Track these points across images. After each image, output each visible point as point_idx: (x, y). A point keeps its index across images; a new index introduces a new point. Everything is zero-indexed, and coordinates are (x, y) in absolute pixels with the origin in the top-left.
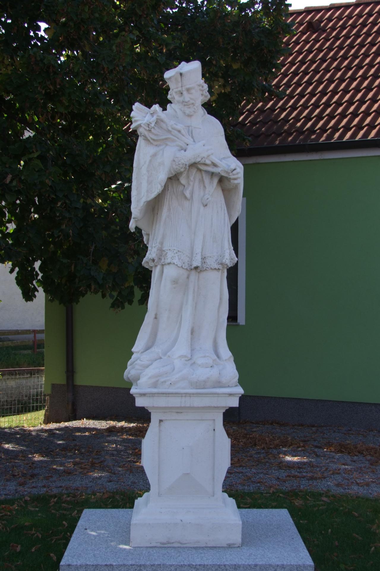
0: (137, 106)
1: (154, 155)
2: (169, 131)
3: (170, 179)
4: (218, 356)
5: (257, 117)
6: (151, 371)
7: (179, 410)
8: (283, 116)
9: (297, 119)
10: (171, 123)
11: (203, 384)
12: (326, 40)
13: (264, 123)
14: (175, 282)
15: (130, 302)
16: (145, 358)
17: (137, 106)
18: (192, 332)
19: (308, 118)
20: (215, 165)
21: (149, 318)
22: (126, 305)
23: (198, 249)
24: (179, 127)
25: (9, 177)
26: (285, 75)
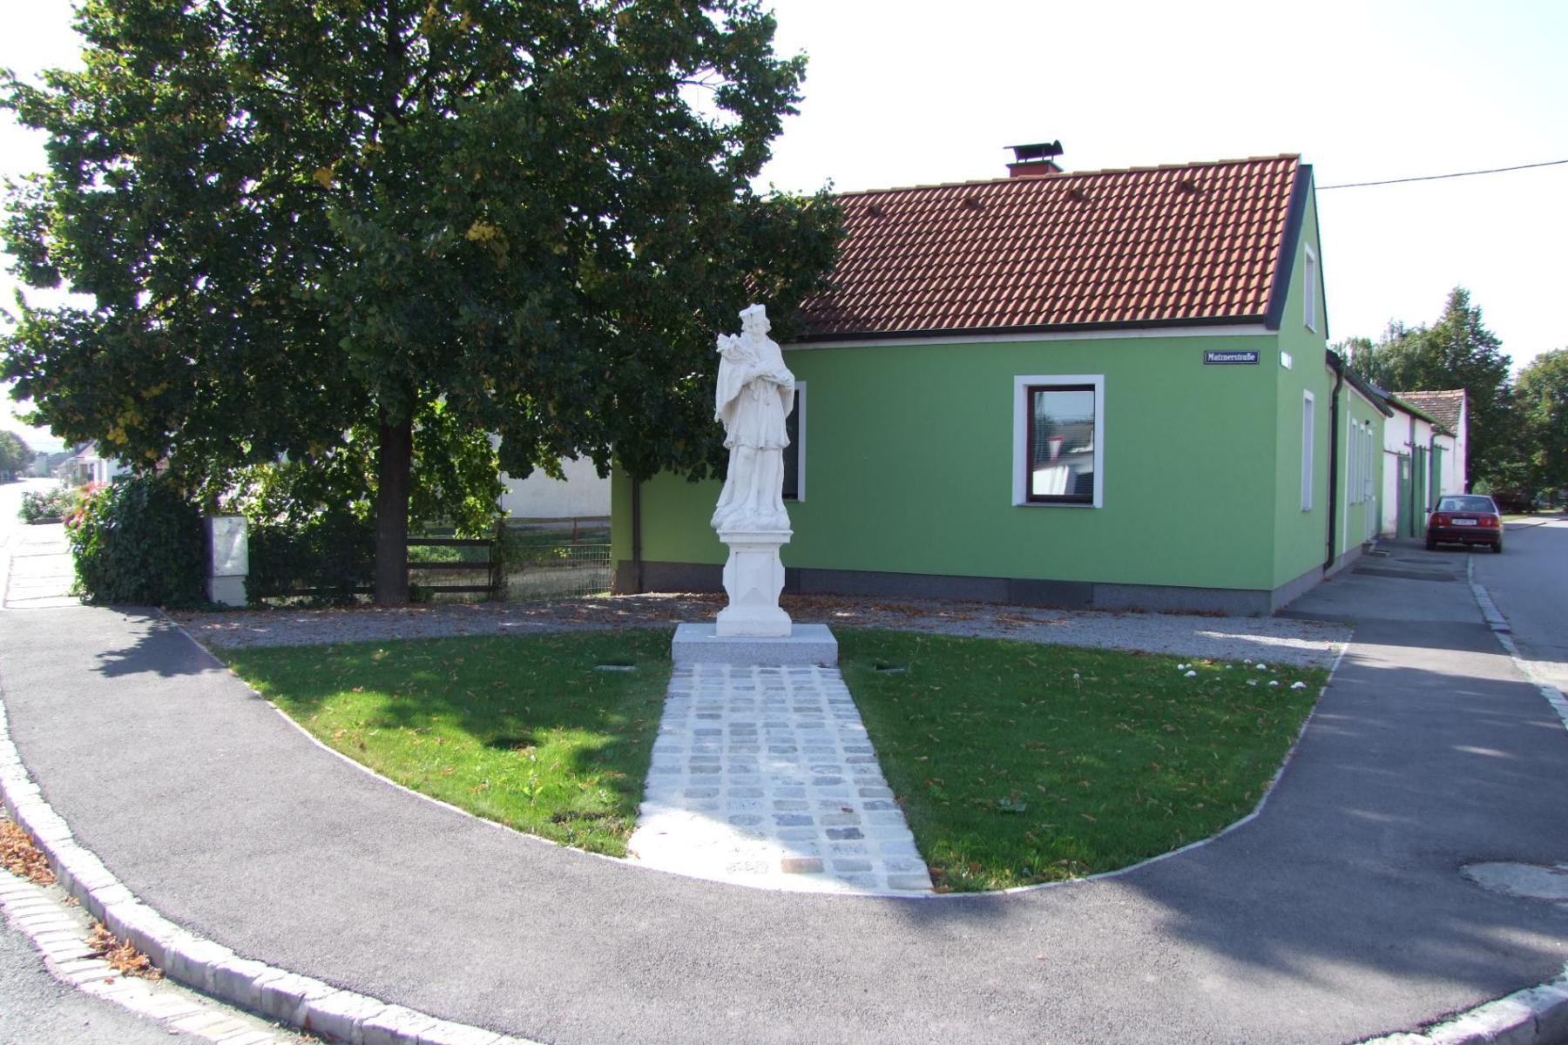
0: (721, 336)
1: (733, 370)
2: (742, 354)
3: (744, 386)
4: (776, 509)
5: (817, 303)
6: (731, 518)
7: (749, 545)
8: (841, 304)
9: (854, 307)
10: (744, 348)
11: (765, 527)
12: (886, 225)
13: (823, 310)
14: (747, 458)
15: (703, 477)
16: (727, 510)
17: (721, 336)
18: (759, 492)
19: (865, 307)
20: (774, 377)
21: (728, 483)
22: (700, 479)
23: (763, 436)
24: (751, 350)
25: (608, 373)
26: (845, 261)
